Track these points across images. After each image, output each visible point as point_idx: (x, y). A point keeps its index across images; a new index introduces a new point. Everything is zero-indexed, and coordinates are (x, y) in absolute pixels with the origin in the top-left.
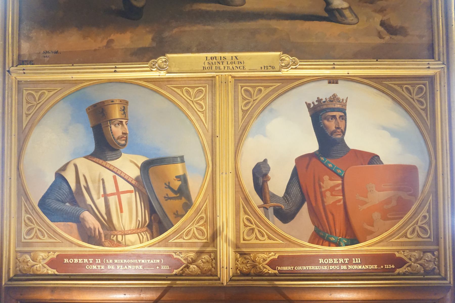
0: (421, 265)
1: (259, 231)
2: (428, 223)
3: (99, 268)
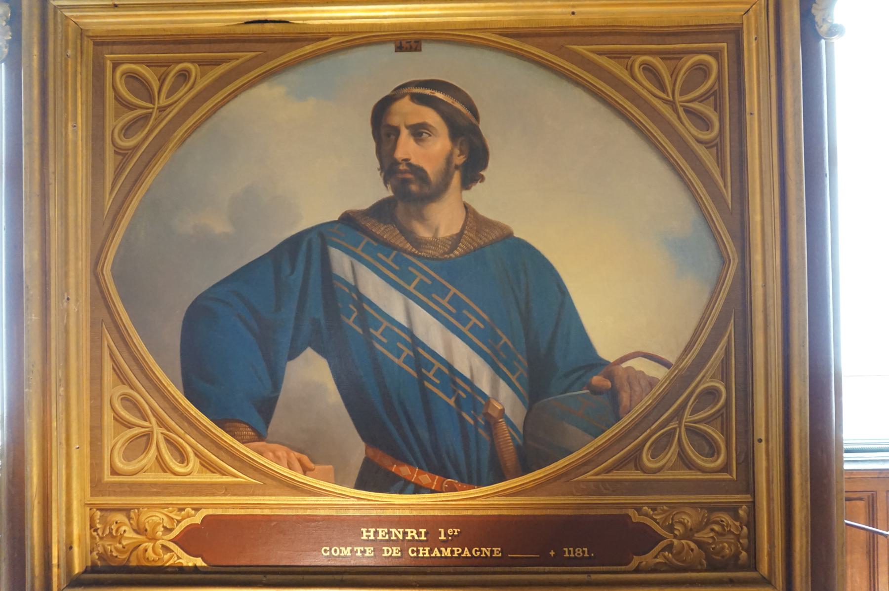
0: (700, 544)
1: (168, 441)
2: (722, 418)
3: (359, 554)
